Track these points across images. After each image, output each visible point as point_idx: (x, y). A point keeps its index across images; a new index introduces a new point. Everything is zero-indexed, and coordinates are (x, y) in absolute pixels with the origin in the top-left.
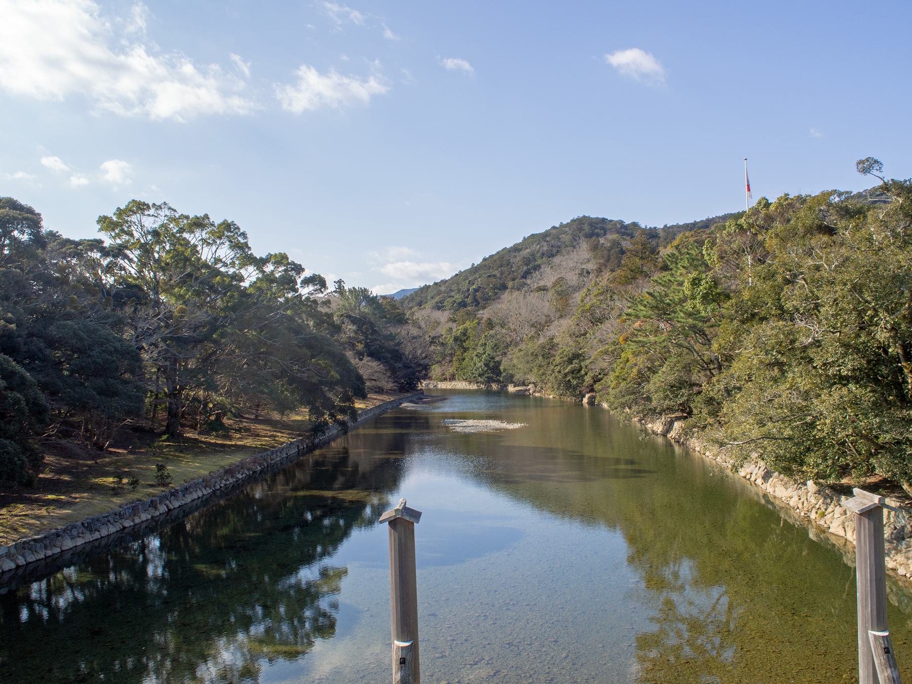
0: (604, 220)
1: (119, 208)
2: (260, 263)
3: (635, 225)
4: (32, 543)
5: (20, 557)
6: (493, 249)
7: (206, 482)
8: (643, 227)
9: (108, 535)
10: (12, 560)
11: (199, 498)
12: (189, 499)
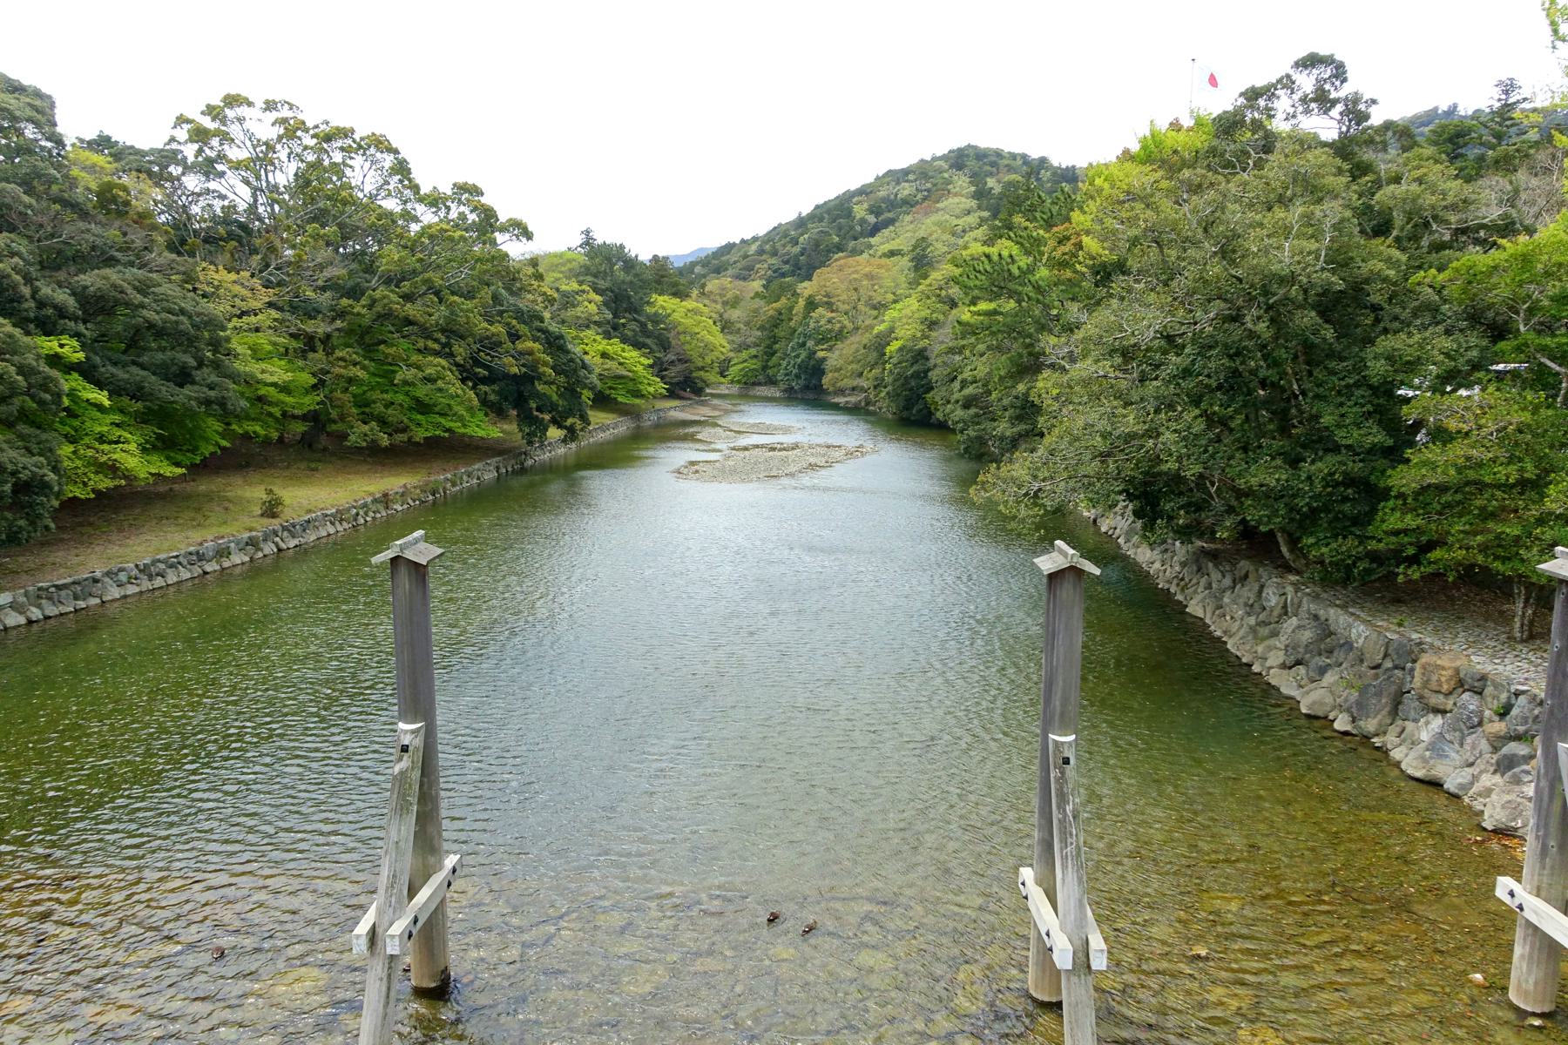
0: (998, 154)
1: (1177, 120)
2: (434, 201)
3: (1043, 161)
4: (53, 589)
5: (34, 609)
6: (829, 191)
7: (339, 517)
8: (1056, 164)
9: (178, 582)
10: (21, 613)
11: (329, 535)
12: (311, 537)
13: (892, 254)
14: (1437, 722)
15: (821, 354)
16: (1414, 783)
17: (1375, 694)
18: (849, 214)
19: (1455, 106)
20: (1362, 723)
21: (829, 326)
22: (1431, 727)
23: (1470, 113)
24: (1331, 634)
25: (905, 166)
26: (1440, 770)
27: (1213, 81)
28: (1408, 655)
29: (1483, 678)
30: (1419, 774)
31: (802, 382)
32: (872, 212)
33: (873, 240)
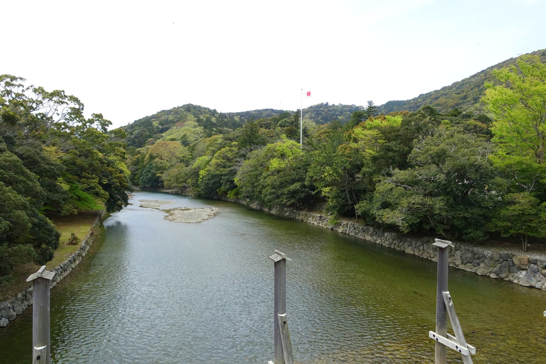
0: (199, 107)
13: (172, 140)
14: (524, 273)
15: (158, 175)
16: (527, 288)
17: (504, 267)
18: (151, 124)
19: (327, 103)
20: (500, 275)
21: (161, 165)
22: (522, 274)
23: (331, 105)
24: (475, 254)
25: (169, 109)
26: (533, 283)
27: (309, 94)
28: (510, 257)
29: (536, 260)
30: (528, 285)
31: (150, 185)
32: (160, 125)
33: (164, 134)
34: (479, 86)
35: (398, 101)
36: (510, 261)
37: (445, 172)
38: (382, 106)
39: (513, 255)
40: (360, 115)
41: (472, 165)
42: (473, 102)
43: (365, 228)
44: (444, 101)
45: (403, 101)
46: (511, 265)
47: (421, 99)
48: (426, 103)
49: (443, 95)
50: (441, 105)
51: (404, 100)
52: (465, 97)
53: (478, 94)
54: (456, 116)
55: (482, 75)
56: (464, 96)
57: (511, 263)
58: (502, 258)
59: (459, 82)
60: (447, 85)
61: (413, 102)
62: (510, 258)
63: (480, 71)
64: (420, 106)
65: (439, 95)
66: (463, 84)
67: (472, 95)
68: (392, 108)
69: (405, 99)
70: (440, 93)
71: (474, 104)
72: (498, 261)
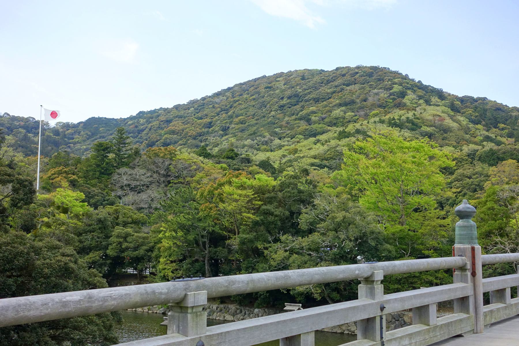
34: (227, 111)
35: (105, 118)
36: (402, 320)
37: (353, 239)
38: (79, 123)
39: (404, 315)
40: (107, 148)
41: (372, 233)
42: (221, 132)
43: (222, 306)
44: (181, 128)
45: (113, 119)
46: (403, 323)
47: (145, 120)
48: (152, 126)
49: (176, 117)
50: (178, 133)
51: (115, 118)
52: (210, 125)
53: (227, 122)
54: (232, 158)
55: (228, 94)
56: (209, 122)
57: (402, 322)
58: (394, 318)
59: (198, 100)
60: (181, 103)
61: (132, 124)
62: (401, 318)
63: (226, 88)
64: (143, 130)
65: (170, 116)
66: (203, 105)
67: (219, 122)
68: (97, 129)
69: (117, 116)
70: (172, 113)
71: (222, 136)
72: (391, 321)
